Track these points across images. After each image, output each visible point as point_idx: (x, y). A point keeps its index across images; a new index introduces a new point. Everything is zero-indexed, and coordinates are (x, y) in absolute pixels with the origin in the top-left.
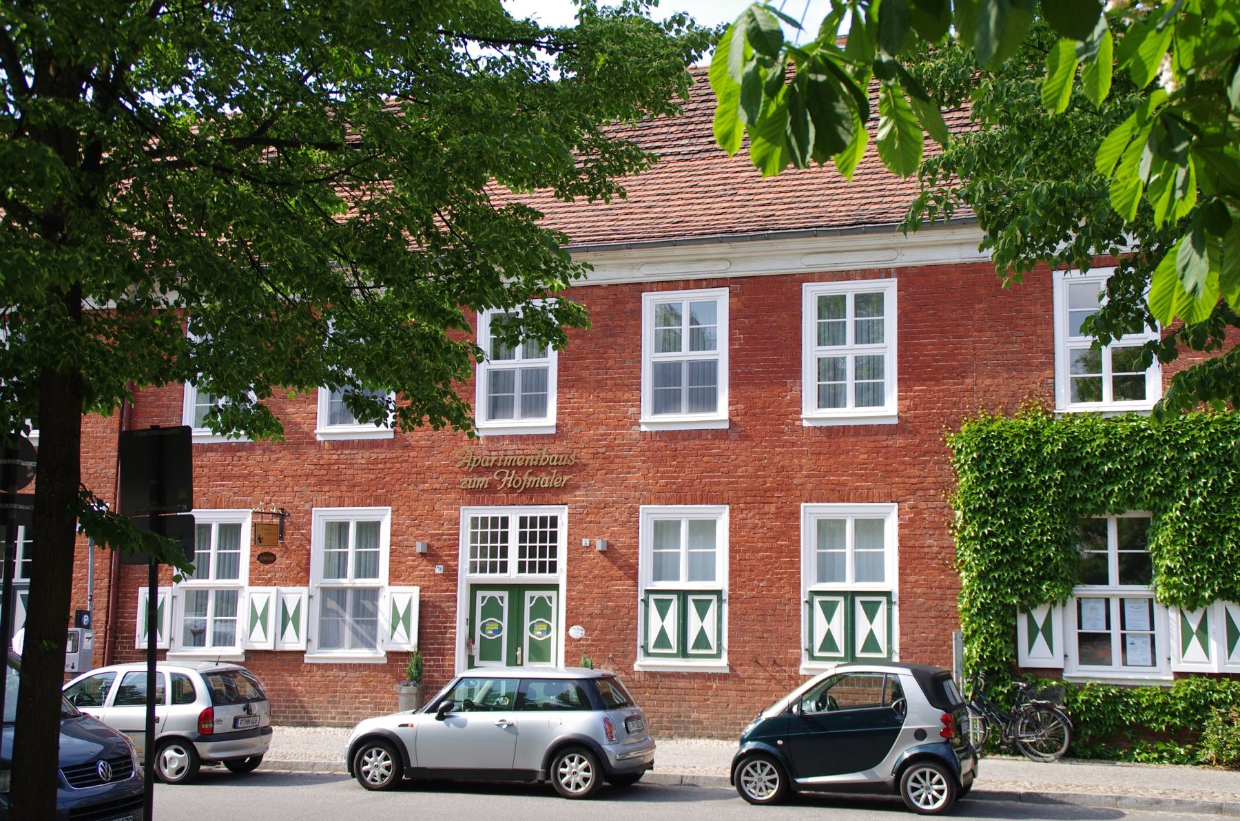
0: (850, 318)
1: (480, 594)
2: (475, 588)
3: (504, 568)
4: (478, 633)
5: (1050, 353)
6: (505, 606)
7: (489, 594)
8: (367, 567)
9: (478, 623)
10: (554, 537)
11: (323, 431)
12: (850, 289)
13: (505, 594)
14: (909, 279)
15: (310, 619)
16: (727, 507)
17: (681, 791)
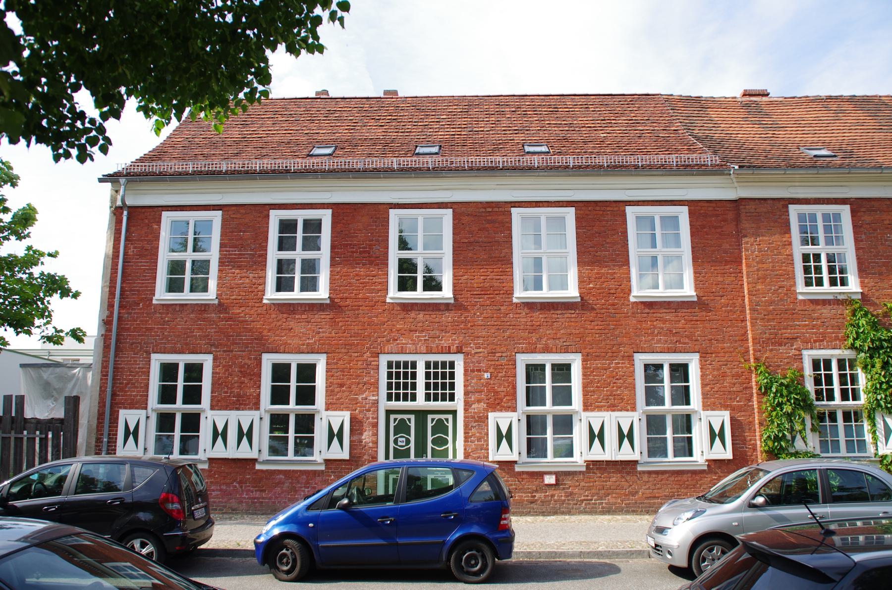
0: (300, 235)
1: (392, 417)
2: (389, 412)
3: (414, 398)
4: (392, 445)
5: (264, 257)
6: (412, 425)
7: (399, 417)
8: (563, 396)
9: (392, 438)
10: (452, 376)
11: (801, 291)
12: (300, 216)
13: (412, 417)
14: (697, 209)
15: (263, 435)
16: (325, 356)
17: (228, 562)
